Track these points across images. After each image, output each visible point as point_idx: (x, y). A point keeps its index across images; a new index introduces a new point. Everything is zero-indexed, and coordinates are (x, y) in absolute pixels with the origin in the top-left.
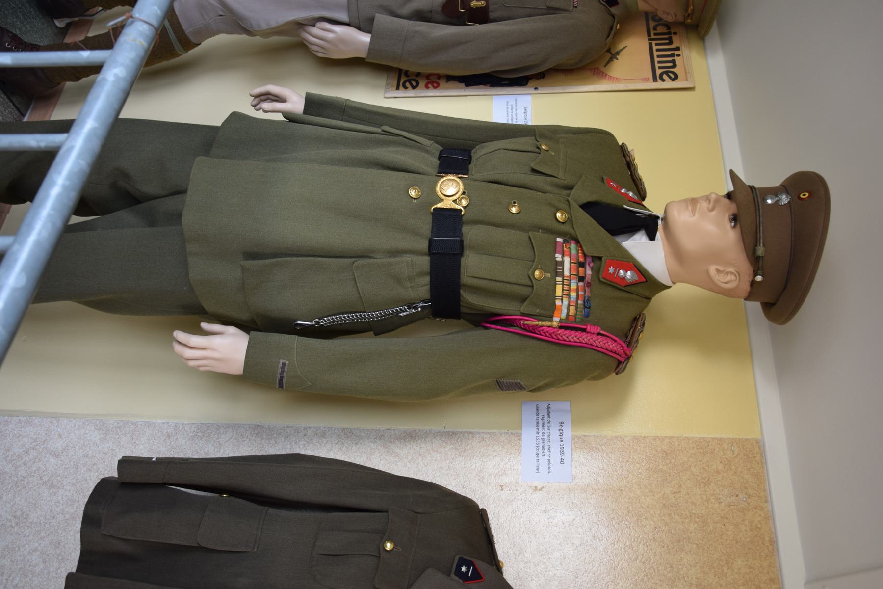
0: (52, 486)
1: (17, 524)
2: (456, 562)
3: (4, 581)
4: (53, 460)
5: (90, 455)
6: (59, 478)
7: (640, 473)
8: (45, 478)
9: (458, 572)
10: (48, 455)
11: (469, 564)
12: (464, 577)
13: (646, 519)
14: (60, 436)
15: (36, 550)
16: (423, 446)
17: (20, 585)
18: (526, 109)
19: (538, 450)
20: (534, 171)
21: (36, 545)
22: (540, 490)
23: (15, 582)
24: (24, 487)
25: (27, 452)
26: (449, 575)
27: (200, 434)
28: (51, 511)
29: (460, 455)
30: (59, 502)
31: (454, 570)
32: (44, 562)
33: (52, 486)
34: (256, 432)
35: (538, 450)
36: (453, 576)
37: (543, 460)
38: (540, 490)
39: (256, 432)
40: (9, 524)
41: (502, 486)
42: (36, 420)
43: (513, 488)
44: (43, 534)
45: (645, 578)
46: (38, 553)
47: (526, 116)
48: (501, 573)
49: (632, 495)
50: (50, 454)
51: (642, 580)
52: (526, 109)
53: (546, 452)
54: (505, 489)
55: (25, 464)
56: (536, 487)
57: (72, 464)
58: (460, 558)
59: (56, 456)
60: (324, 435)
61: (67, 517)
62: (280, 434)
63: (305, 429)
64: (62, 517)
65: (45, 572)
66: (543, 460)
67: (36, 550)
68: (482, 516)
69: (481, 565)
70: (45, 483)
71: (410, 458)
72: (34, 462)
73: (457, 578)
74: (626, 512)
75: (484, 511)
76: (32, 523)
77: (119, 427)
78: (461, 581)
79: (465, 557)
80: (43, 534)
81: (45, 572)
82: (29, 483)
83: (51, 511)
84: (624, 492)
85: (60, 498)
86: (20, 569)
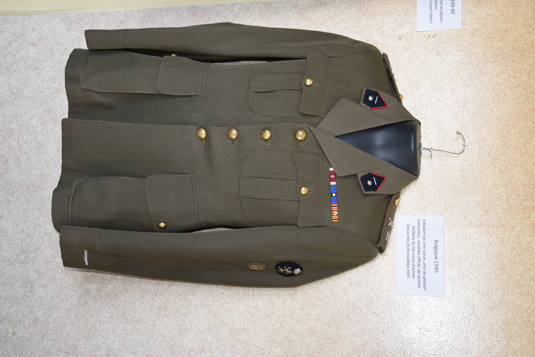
0: (36, 68)
1: (15, 99)
2: (364, 93)
3: (17, 139)
4: (32, 49)
5: (61, 43)
6: (40, 62)
7: (526, 15)
8: (30, 63)
9: (366, 101)
10: (27, 45)
11: (374, 94)
12: (371, 104)
13: (529, 53)
14: (34, 29)
15: (34, 116)
16: (331, 10)
17: (28, 141)
18: (436, 241)
19: (431, 4)
20: (436, 269)
21: (33, 112)
22: (433, 37)
23: (24, 139)
24: (14, 71)
25: (10, 44)
26: (359, 102)
27: (146, 18)
28: (39, 87)
29: (364, 15)
30: (44, 80)
31: (362, 99)
32: (42, 124)
33: (36, 68)
34: (192, 12)
35: (431, 4)
36: (362, 104)
37: (436, 12)
38: (433, 37)
39: (192, 12)
40: (9, 99)
41: (399, 37)
42: (11, 18)
43: (409, 38)
44: (37, 104)
45: (526, 102)
46: (36, 118)
47: (436, 253)
48: (401, 103)
49: (517, 34)
50: (29, 44)
51: (523, 103)
52: (436, 241)
53: (439, 5)
54: (403, 39)
55: (11, 54)
56: (429, 35)
57: (48, 50)
58: (368, 91)
59: (34, 45)
60: (248, 9)
61: (53, 90)
62: (212, 11)
63: (232, 5)
64: (49, 92)
65: (45, 131)
66: (436, 12)
67: (34, 116)
68: (384, 60)
69: (385, 96)
70: (30, 67)
71: (321, 21)
72: (18, 52)
73: (365, 105)
74: (511, 49)
75: (385, 55)
76: (26, 97)
77: (80, 19)
78: (369, 107)
79: (372, 89)
80: (37, 104)
81: (45, 131)
82: (17, 67)
83: (39, 87)
84: (510, 33)
85: (44, 77)
86: (26, 130)
